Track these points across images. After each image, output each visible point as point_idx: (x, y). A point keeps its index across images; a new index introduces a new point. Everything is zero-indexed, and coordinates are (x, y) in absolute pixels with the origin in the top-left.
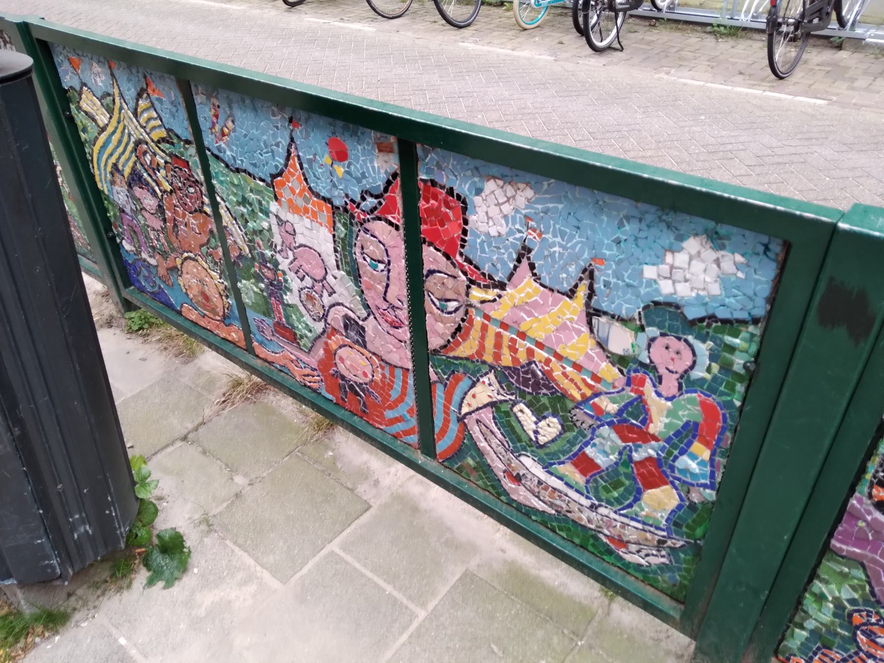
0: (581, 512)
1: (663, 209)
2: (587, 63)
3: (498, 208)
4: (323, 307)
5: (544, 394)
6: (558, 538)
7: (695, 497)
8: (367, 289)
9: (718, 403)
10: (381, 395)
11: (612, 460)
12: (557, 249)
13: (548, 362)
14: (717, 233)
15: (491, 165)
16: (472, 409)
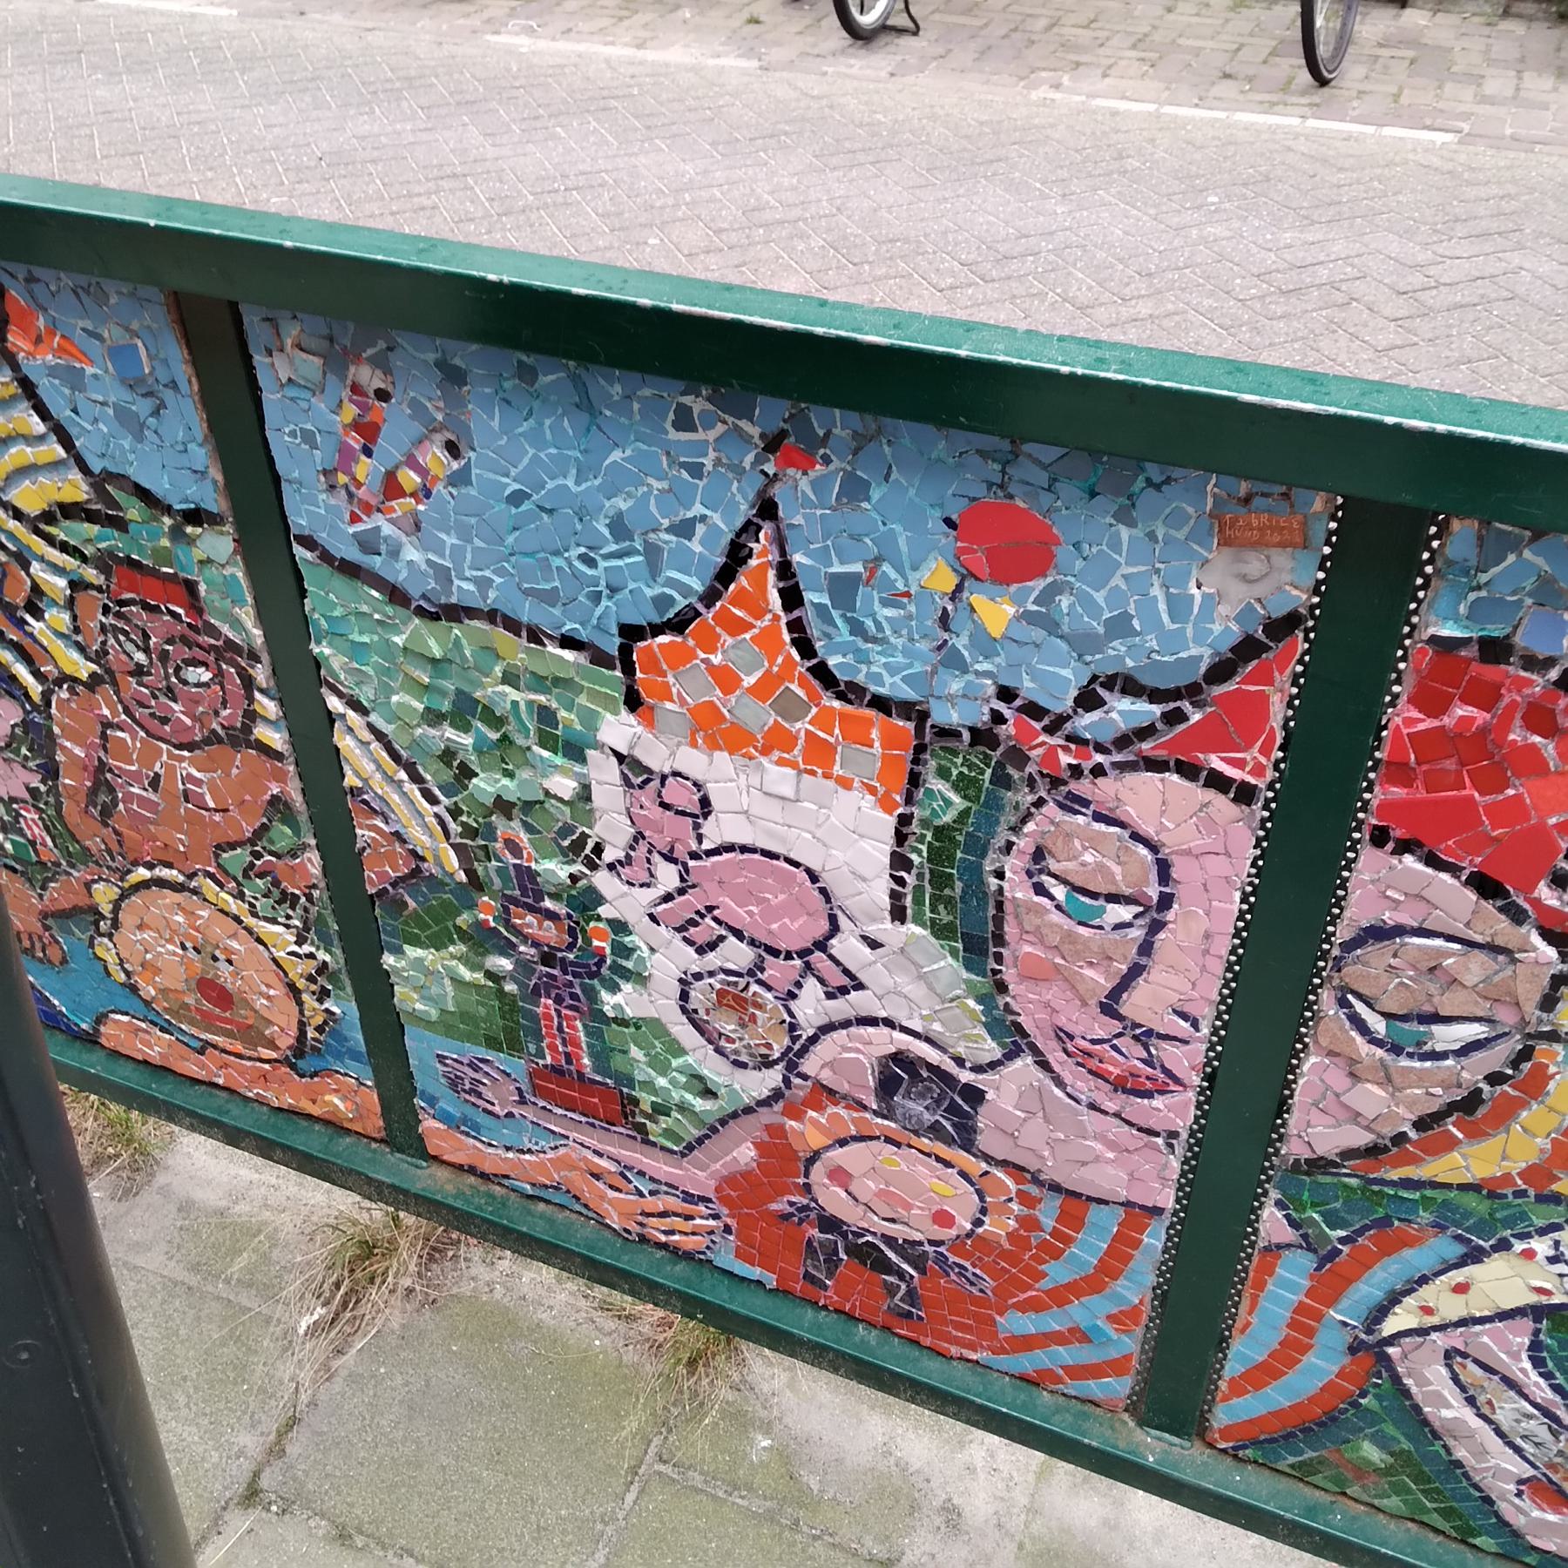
2: (843, 69)
4: (793, 1027)
8: (1024, 977)
10: (995, 1273)
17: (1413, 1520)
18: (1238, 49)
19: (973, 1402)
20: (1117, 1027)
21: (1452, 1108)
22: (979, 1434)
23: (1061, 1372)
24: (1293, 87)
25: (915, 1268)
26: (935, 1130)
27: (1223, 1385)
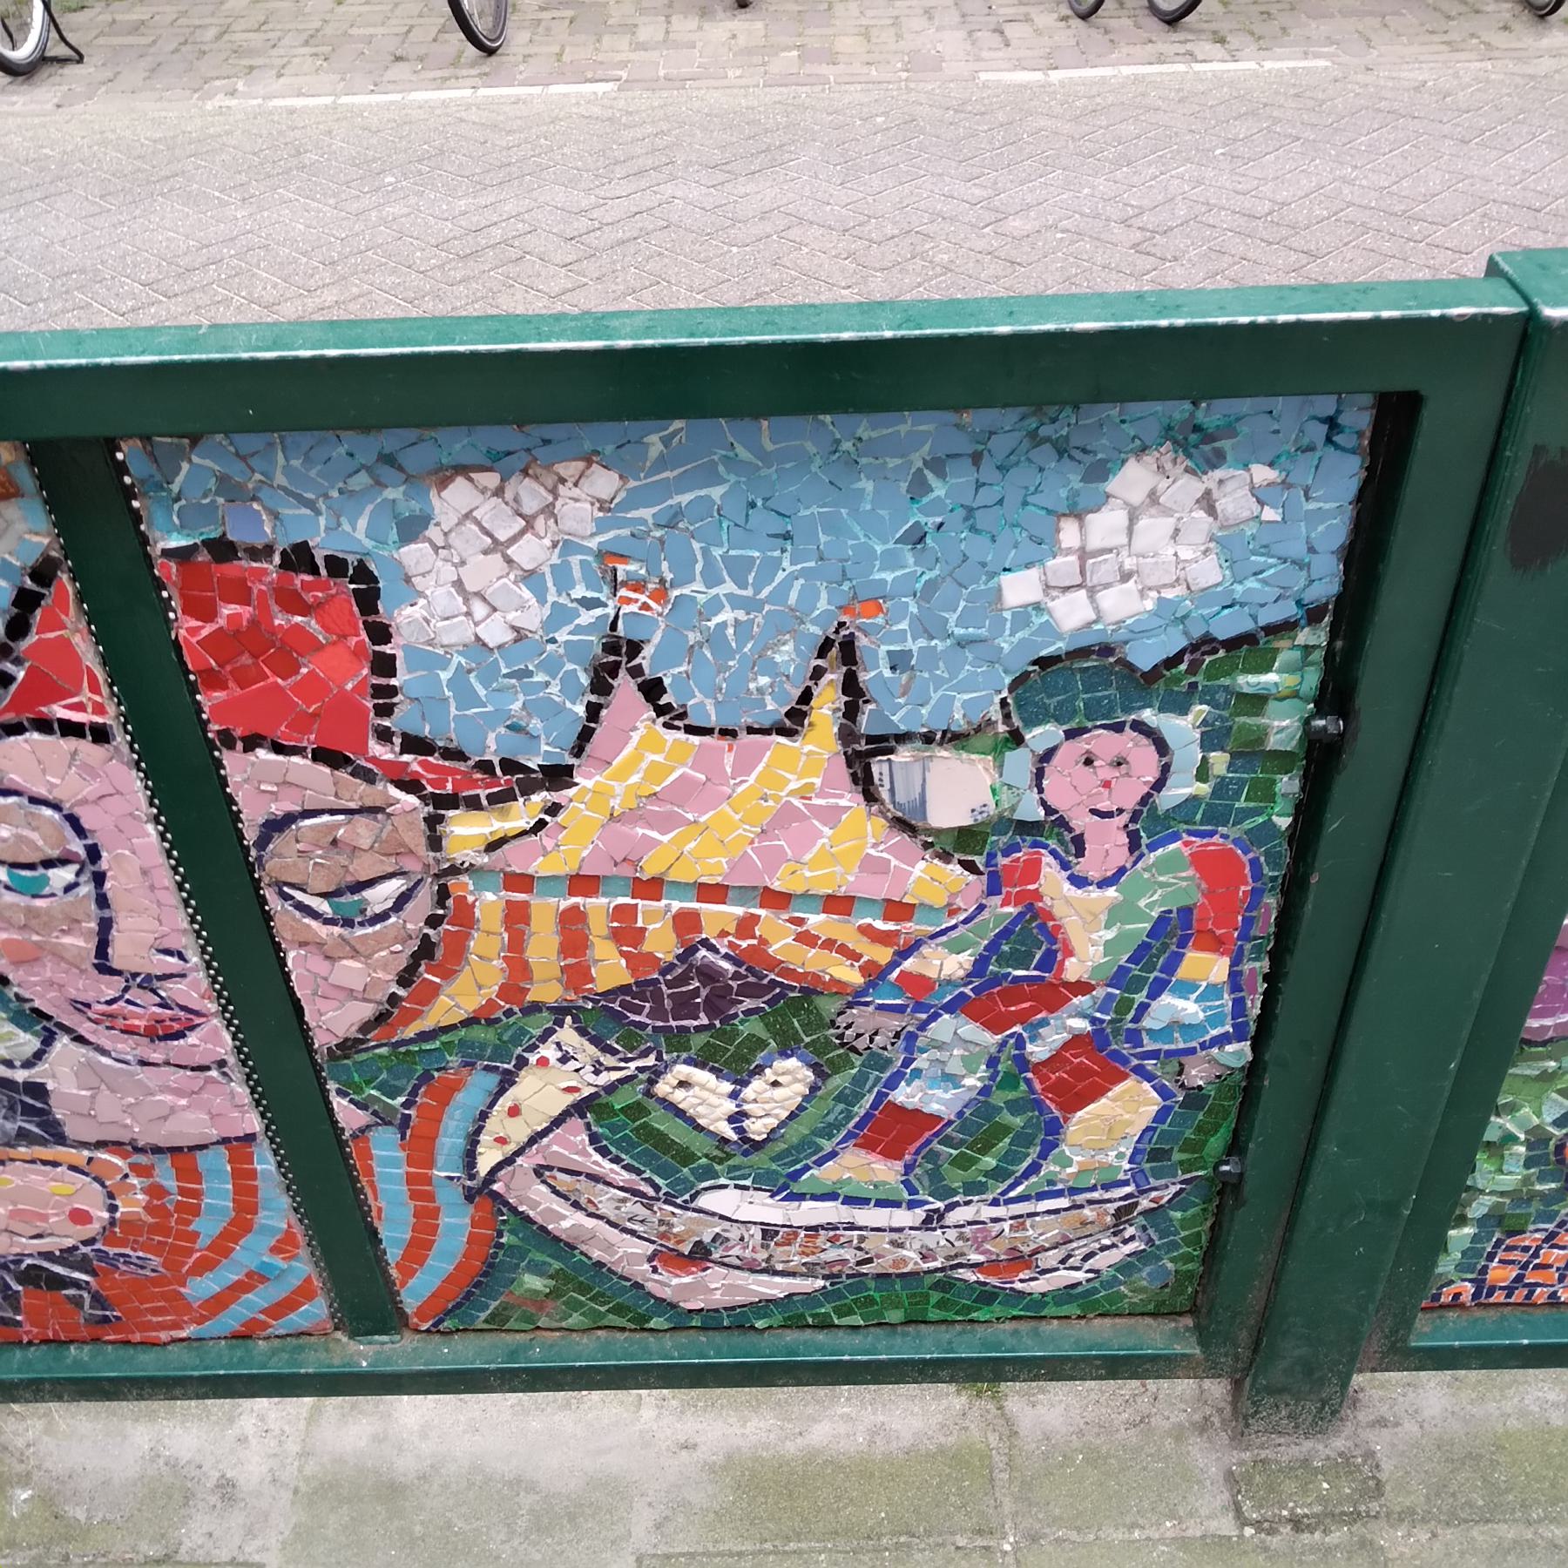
0: (901, 1246)
1: (1038, 406)
3: (497, 558)
5: (748, 1012)
6: (843, 1338)
7: (1197, 1075)
9: (1235, 842)
10: (158, 1249)
11: (970, 1088)
12: (726, 615)
13: (746, 926)
14: (1197, 428)
15: (442, 434)
16: (511, 1148)
17: (599, 1328)
18: (409, 31)
19: (191, 1377)
20: (120, 982)
21: (416, 958)
22: (247, 1403)
23: (262, 1317)
24: (462, 60)
25: (86, 1272)
26: (23, 1136)
27: (394, 1273)
